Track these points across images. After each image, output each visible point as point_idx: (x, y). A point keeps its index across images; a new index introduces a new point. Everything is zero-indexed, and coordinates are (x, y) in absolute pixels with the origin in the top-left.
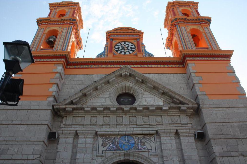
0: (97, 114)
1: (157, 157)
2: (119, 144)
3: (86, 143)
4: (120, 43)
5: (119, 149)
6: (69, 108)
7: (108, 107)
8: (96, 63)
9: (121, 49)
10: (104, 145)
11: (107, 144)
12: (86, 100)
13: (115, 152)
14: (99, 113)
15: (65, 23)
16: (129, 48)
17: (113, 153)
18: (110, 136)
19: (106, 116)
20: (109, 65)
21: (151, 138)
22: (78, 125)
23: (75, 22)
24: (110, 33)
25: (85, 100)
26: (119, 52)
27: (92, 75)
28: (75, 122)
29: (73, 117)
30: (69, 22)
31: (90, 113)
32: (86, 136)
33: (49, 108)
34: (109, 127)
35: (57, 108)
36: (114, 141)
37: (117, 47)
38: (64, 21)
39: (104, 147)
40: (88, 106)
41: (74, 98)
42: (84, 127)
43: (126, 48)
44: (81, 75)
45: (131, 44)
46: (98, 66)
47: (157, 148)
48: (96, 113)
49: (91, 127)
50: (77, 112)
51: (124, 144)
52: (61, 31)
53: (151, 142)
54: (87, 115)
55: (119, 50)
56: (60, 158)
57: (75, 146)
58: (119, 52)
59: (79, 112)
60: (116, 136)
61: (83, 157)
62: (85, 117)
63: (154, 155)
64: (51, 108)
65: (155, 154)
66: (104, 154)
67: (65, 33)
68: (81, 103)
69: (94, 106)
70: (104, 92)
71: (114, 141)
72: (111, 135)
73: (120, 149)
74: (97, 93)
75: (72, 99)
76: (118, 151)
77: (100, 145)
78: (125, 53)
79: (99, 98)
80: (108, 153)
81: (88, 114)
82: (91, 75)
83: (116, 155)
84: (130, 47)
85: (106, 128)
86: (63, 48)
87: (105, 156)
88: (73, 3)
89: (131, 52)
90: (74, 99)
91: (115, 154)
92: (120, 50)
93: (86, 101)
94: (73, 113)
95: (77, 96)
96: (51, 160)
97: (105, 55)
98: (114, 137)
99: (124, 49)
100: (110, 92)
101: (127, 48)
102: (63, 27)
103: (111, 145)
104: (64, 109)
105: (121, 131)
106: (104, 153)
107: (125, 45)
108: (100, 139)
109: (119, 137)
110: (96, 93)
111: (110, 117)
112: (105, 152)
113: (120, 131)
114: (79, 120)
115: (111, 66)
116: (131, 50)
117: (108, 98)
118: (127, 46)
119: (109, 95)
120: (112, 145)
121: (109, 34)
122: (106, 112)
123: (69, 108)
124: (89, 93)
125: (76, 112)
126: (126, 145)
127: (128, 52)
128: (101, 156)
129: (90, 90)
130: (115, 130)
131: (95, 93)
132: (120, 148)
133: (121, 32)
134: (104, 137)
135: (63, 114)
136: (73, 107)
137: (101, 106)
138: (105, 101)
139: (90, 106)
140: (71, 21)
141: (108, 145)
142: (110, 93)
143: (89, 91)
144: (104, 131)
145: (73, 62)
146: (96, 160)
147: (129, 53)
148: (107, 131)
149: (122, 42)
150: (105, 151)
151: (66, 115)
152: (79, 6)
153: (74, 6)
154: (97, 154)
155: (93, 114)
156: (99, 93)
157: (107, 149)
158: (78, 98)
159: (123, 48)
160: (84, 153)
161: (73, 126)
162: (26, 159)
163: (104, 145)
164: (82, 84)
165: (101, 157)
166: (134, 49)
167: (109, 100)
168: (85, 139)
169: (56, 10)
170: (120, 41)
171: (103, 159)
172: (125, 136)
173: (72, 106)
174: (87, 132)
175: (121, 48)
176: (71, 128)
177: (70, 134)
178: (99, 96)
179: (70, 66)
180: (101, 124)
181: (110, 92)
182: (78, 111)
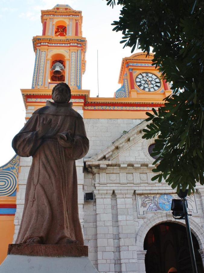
0: (133, 170)
1: (199, 218)
2: (159, 203)
3: (125, 204)
4: (141, 75)
5: (159, 209)
6: (103, 164)
7: (146, 163)
8: (120, 104)
9: (144, 84)
10: (144, 205)
11: (147, 204)
12: (118, 153)
13: (157, 213)
14: (135, 170)
15: (71, 44)
16: (153, 82)
17: (154, 214)
18: (149, 195)
19: (142, 172)
20: (135, 107)
21: (191, 196)
22: (114, 183)
23: (84, 43)
24: (128, 61)
25: (116, 153)
26: (142, 88)
27: (117, 119)
28: (110, 179)
29: (107, 173)
30: (77, 43)
31: (126, 170)
32: (124, 196)
33: (81, 165)
34: (147, 186)
35: (89, 165)
36: (154, 200)
37: (138, 80)
38: (69, 41)
39: (144, 207)
40: (124, 163)
41: (107, 152)
42: (121, 185)
43: (149, 83)
44: (103, 119)
45: (154, 77)
46: (122, 108)
47: (198, 208)
48: (131, 170)
49: (128, 185)
50: (112, 169)
51: (164, 204)
52: (70, 57)
53: (192, 201)
54: (122, 172)
55: (142, 84)
56: (101, 221)
57: (114, 207)
58: (142, 88)
59: (113, 169)
60: (155, 195)
61: (125, 219)
62: (120, 174)
63: (195, 216)
64: (83, 165)
65: (196, 214)
66: (145, 215)
67: (75, 60)
68: (112, 157)
69: (131, 163)
70: (136, 143)
71: (154, 200)
72: (150, 194)
73: (161, 210)
74: (129, 144)
75: (105, 154)
76: (159, 211)
77: (140, 205)
78: (150, 90)
79: (131, 151)
80: (149, 214)
81: (123, 171)
82: (115, 120)
83: (158, 216)
84: (154, 80)
85: (144, 186)
86: (77, 83)
87: (146, 217)
88: (74, 12)
89: (156, 88)
90: (107, 154)
91: (157, 215)
92: (143, 85)
93: (118, 155)
94: (107, 170)
95: (109, 150)
96: (91, 224)
97: (126, 92)
98: (153, 196)
99: (148, 84)
100: (142, 143)
101: (151, 82)
102: (70, 50)
103: (151, 204)
104: (98, 166)
105: (161, 190)
106: (145, 214)
107: (147, 77)
108: (139, 198)
109: (158, 196)
110: (127, 145)
111: (146, 173)
112: (146, 213)
113: (159, 190)
114: (113, 177)
115: (137, 108)
116: (156, 86)
117: (141, 150)
118: (150, 79)
119: (142, 147)
120: (152, 205)
121: (126, 61)
122: (143, 169)
123: (103, 164)
124: (121, 145)
125: (110, 169)
126: (167, 205)
127: (153, 88)
128: (142, 217)
129: (123, 143)
130: (154, 189)
131: (127, 145)
132: (161, 209)
133: (142, 59)
134: (143, 196)
135: (95, 170)
136: (107, 163)
137: (139, 163)
138: (138, 155)
139: (127, 163)
140: (79, 41)
141: (148, 206)
142: (142, 145)
143: (122, 144)
144: (143, 190)
145: (92, 102)
146: (138, 222)
147: (154, 89)
148: (146, 190)
149: (143, 73)
150: (146, 212)
151: (99, 171)
152: (81, 15)
153: (75, 15)
154: (139, 216)
155: (129, 171)
156: (131, 145)
157: (147, 209)
158: (110, 152)
159: (146, 82)
160: (126, 215)
161: (108, 185)
162: (132, 258)
163: (144, 205)
164: (107, 132)
165: (142, 218)
166: (158, 84)
167: (143, 154)
168: (123, 199)
169: (53, 21)
170: (141, 72)
171: (145, 220)
172: (164, 195)
173: (107, 162)
174: (125, 191)
175: (143, 82)
176: (107, 186)
177: (107, 193)
178: (131, 148)
179: (88, 106)
180: (138, 181)
181: (142, 143)
182: (112, 168)
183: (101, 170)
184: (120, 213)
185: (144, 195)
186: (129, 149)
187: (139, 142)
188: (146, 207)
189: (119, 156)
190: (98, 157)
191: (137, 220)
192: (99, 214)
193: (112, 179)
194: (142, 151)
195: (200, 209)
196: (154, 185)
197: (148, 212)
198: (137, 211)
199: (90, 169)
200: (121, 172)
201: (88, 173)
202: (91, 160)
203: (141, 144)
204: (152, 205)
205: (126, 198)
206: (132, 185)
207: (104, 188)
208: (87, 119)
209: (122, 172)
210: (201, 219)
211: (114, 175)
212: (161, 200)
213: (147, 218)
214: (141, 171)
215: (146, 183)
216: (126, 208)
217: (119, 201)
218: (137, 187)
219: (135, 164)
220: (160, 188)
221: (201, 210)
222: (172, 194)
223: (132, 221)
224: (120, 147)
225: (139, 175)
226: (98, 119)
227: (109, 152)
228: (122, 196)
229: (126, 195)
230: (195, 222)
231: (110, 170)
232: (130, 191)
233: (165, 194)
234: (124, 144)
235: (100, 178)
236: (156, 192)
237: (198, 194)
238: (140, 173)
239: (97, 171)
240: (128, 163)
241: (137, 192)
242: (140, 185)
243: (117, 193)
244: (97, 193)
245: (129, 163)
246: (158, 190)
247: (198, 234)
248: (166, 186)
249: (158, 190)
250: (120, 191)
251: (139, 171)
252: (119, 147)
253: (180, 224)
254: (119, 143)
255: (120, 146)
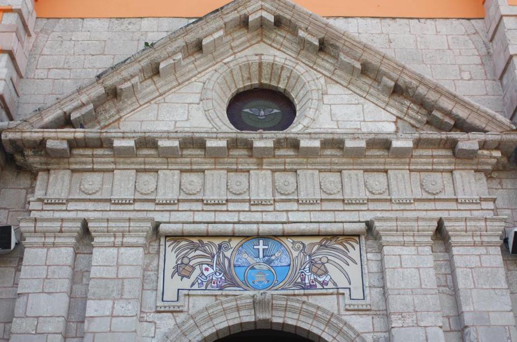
0: (159, 160)
1: (368, 315)
3: (118, 265)
5: (234, 284)
7: (197, 135)
10: (182, 270)
11: (193, 268)
12: (118, 112)
13: (222, 295)
18: (205, 241)
19: (188, 167)
22: (90, 200)
28: (80, 189)
31: (135, 160)
32: (119, 240)
36: (219, 257)
39: (183, 277)
40: (126, 135)
41: (75, 104)
42: (113, 207)
47: (367, 284)
48: (153, 160)
49: (137, 206)
50: (87, 156)
51: (253, 268)
54: (121, 167)
56: (27, 317)
57: (79, 275)
59: (93, 156)
60: (227, 240)
62: (115, 171)
66: (183, 301)
69: (147, 135)
71: (219, 257)
72: (208, 235)
73: (239, 286)
74: (158, 85)
75: (67, 109)
77: (170, 270)
79: (165, 104)
81: (124, 163)
82: (133, 20)
83: (225, 306)
85: (190, 211)
87: (185, 309)
90: (76, 109)
93: (117, 117)
94: (72, 160)
98: (217, 242)
103: (207, 269)
104: (40, 146)
106: (182, 298)
108: (169, 249)
109: (234, 243)
110: (153, 87)
111: (203, 171)
112: (185, 295)
113: (239, 222)
114: (92, 182)
120: (211, 271)
122: (191, 156)
124: (127, 85)
125: (82, 156)
126: (261, 272)
128: (172, 309)
129: (132, 77)
130: (223, 220)
131: (149, 87)
134: (184, 243)
135: (34, 160)
136: (70, 136)
141: (197, 272)
142: (203, 88)
143: (129, 80)
144: (183, 223)
148: (194, 223)
150: (186, 292)
154: (160, 303)
155: (145, 163)
156: (165, 88)
157: (193, 284)
160: (114, 300)
161: (71, 206)
163: (182, 270)
165: (172, 312)
167: (201, 114)
168: (115, 250)
171: (181, 317)
172: (255, 241)
173: (69, 133)
174: (122, 224)
176: (66, 210)
177: (61, 231)
178: (164, 99)
181: (204, 83)
182: (88, 152)
183: (53, 161)
184: (94, 294)
185: (186, 240)
186: (157, 99)
187: (193, 79)
188: (188, 277)
189: (123, 119)
190: (42, 119)
191: (152, 317)
192: (25, 297)
193: (86, 186)
194: (201, 105)
195: (375, 287)
196: (224, 208)
197: (191, 292)
198: (156, 290)
199: (18, 157)
200: (118, 167)
201: (18, 173)
202: (20, 127)
203: (201, 84)
204: (211, 271)
205: (122, 245)
206: (151, 206)
207: (57, 215)
208: (48, 18)
209: (121, 167)
210: (376, 319)
211: (97, 178)
212: (245, 256)
213: (188, 312)
214: (186, 164)
215: (197, 201)
216: (117, 278)
217: (99, 255)
218: (167, 214)
219: (161, 138)
220: (243, 217)
221: (378, 290)
222: (284, 239)
223: (130, 319)
224: (121, 89)
225: (176, 177)
226: (80, 20)
227: (83, 105)
228: (112, 239)
229: (123, 236)
230: (351, 328)
231: (84, 159)
232: (138, 224)
233: (259, 236)
234: (136, 80)
235: (50, 187)
236: (229, 228)
237: (376, 239)
238: (182, 171)
239: (41, 164)
240: (140, 134)
241: (163, 228)
242: (175, 207)
243: (95, 232)
244: (27, 229)
245: (143, 134)
246: (234, 223)
247: (225, 325)
248: (262, 211)
249: (234, 223)
250: (105, 225)
251: (176, 163)
252: (118, 91)
253: (304, 335)
254: (120, 77)
255: (123, 87)
